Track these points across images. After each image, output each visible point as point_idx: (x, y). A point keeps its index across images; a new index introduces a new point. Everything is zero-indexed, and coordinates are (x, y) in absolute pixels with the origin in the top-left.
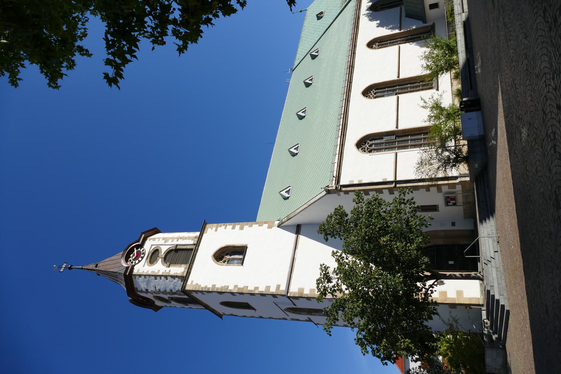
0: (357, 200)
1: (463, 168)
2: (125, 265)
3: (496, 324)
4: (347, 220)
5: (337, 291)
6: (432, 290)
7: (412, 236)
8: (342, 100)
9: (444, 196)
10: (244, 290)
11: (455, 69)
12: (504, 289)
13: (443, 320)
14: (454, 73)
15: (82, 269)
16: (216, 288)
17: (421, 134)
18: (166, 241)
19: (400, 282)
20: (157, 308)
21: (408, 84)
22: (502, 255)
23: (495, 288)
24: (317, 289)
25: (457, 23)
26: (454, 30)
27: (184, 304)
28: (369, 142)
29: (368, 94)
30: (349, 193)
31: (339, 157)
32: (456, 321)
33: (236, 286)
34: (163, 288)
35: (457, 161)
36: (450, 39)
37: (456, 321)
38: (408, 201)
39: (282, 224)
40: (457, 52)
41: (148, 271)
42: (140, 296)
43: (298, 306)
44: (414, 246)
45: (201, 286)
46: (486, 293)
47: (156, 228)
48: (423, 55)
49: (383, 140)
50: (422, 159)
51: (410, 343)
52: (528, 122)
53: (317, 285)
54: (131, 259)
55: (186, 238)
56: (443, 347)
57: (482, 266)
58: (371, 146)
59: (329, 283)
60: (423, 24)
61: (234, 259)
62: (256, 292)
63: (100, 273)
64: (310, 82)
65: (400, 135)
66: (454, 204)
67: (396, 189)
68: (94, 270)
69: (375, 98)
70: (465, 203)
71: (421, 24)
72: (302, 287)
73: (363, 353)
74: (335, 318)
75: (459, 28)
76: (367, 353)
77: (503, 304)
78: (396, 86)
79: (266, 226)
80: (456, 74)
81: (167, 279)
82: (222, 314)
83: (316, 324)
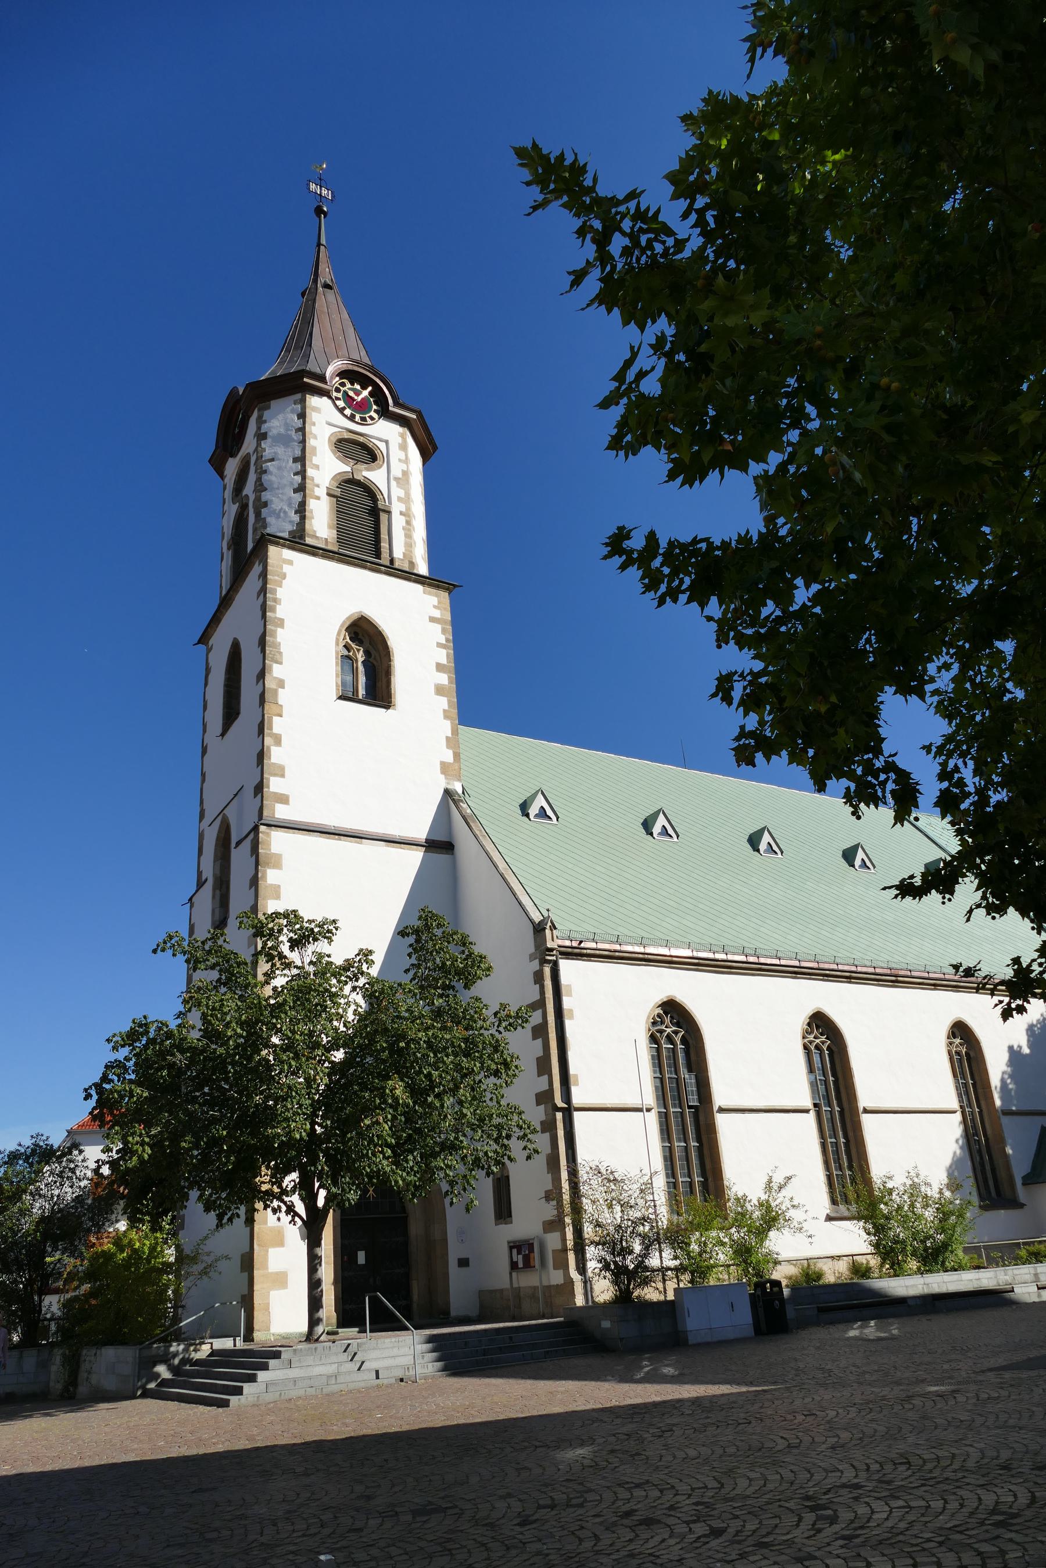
0: (503, 1014)
1: (604, 1290)
2: (329, 371)
5: (270, 964)
6: (280, 1211)
7: (414, 1158)
8: (798, 957)
9: (534, 1239)
10: (273, 706)
11: (882, 1265)
13: (206, 1238)
15: (319, 245)
16: (273, 628)
17: (703, 1173)
20: (218, 464)
21: (846, 1136)
22: (367, 1388)
24: (272, 914)
25: (1010, 1272)
26: (991, 1264)
28: (680, 1035)
29: (818, 1028)
30: (538, 985)
31: (636, 955)
32: (205, 1272)
33: (281, 684)
34: (270, 481)
35: (619, 1274)
36: (966, 1250)
37: (206, 1273)
39: (453, 800)
40: (927, 1271)
41: (315, 438)
42: (249, 417)
44: (386, 1166)
45: (278, 589)
46: (274, 1349)
47: (435, 448)
48: (922, 1177)
49: (686, 1071)
50: (623, 1181)
51: (140, 1157)
52: (645, 1450)
53: (282, 912)
54: (349, 385)
55: (408, 536)
56: (141, 1239)
60: (1023, 1175)
61: (354, 672)
62: (268, 741)
63: (309, 296)
64: (858, 862)
65: (702, 1118)
66: (514, 1266)
68: (315, 281)
69: (805, 1047)
70: (517, 1292)
71: (1020, 1169)
72: (285, 862)
74: (200, 962)
75: (996, 1277)
77: (245, 1391)
78: (840, 1105)
79: (449, 756)
80: (863, 1269)
81: (295, 491)
83: (190, 899)
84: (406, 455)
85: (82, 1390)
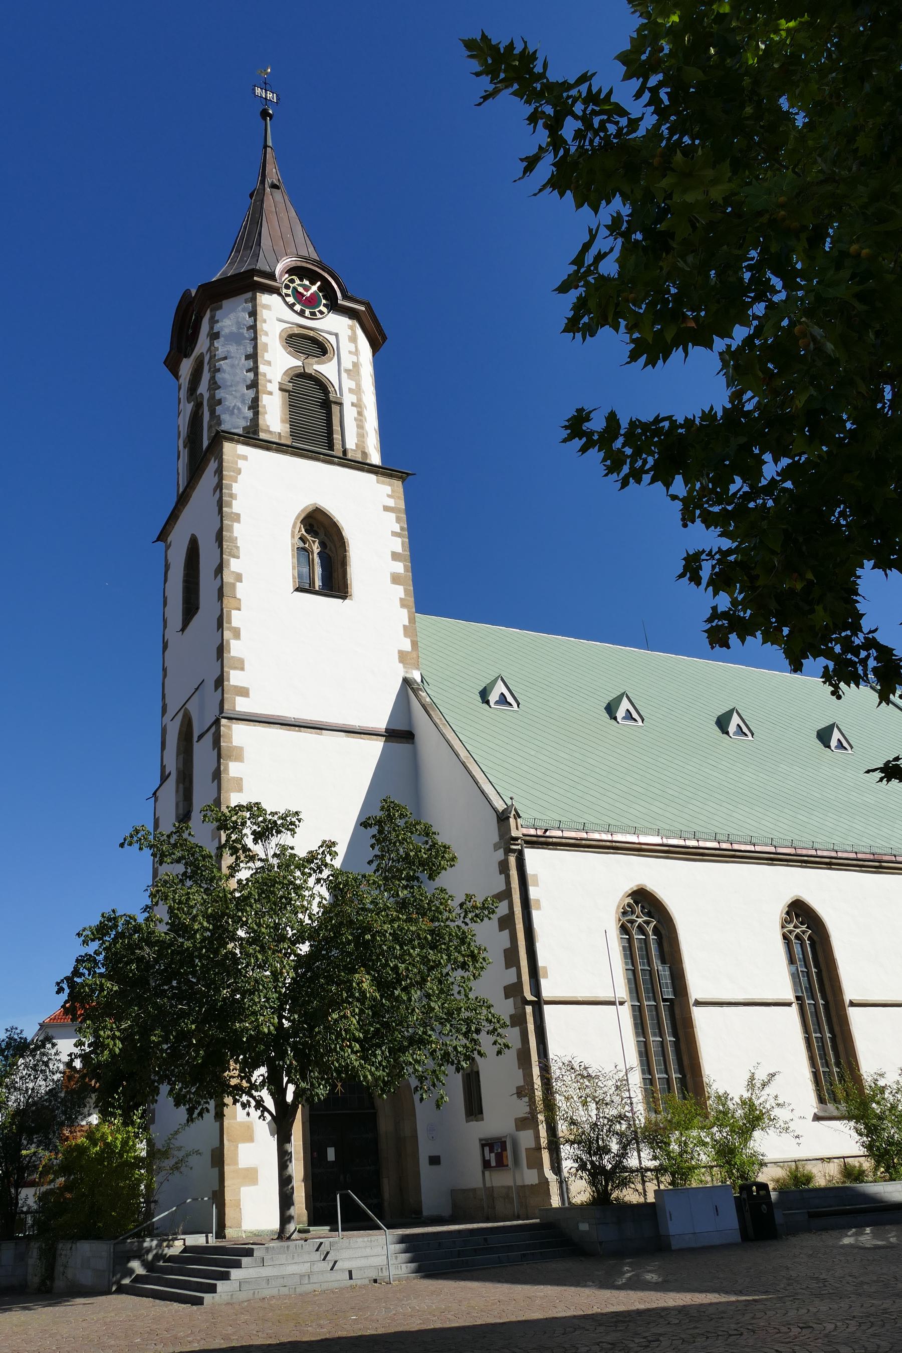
0: (469, 905)
2: (279, 269)
3: (172, 1271)
4: (417, 879)
5: (234, 856)
6: (250, 1106)
7: (383, 1052)
8: (774, 843)
10: (231, 600)
11: (876, 1169)
12: (256, 1293)
13: (177, 1132)
14: (861, 1166)
18: (351, 373)
19: (258, 1026)
20: (173, 365)
21: (831, 1031)
22: (342, 1289)
23: (257, 1269)
24: (235, 807)
27: (188, 436)
28: (652, 925)
29: (797, 916)
31: (604, 843)
32: (176, 1167)
33: (239, 577)
34: (223, 379)
37: (177, 1168)
38: (475, 1041)
39: (412, 689)
42: (202, 318)
43: (196, 746)
44: (355, 1060)
46: (247, 1246)
47: (384, 338)
50: (597, 1077)
53: (245, 805)
54: (298, 282)
55: (360, 426)
57: (322, 1236)
58: (641, 930)
59: (253, 837)
61: (310, 564)
62: (227, 634)
63: (257, 197)
66: (486, 1164)
67: (520, 1005)
68: (263, 182)
69: (785, 937)
70: (490, 1192)
73: (84, 930)
74: (166, 856)
76: (84, 942)
77: (219, 1289)
78: (824, 997)
79: (406, 645)
80: (856, 1172)
81: (248, 387)
82: (169, 540)
83: (155, 794)
84: (356, 347)
85: (59, 1283)
